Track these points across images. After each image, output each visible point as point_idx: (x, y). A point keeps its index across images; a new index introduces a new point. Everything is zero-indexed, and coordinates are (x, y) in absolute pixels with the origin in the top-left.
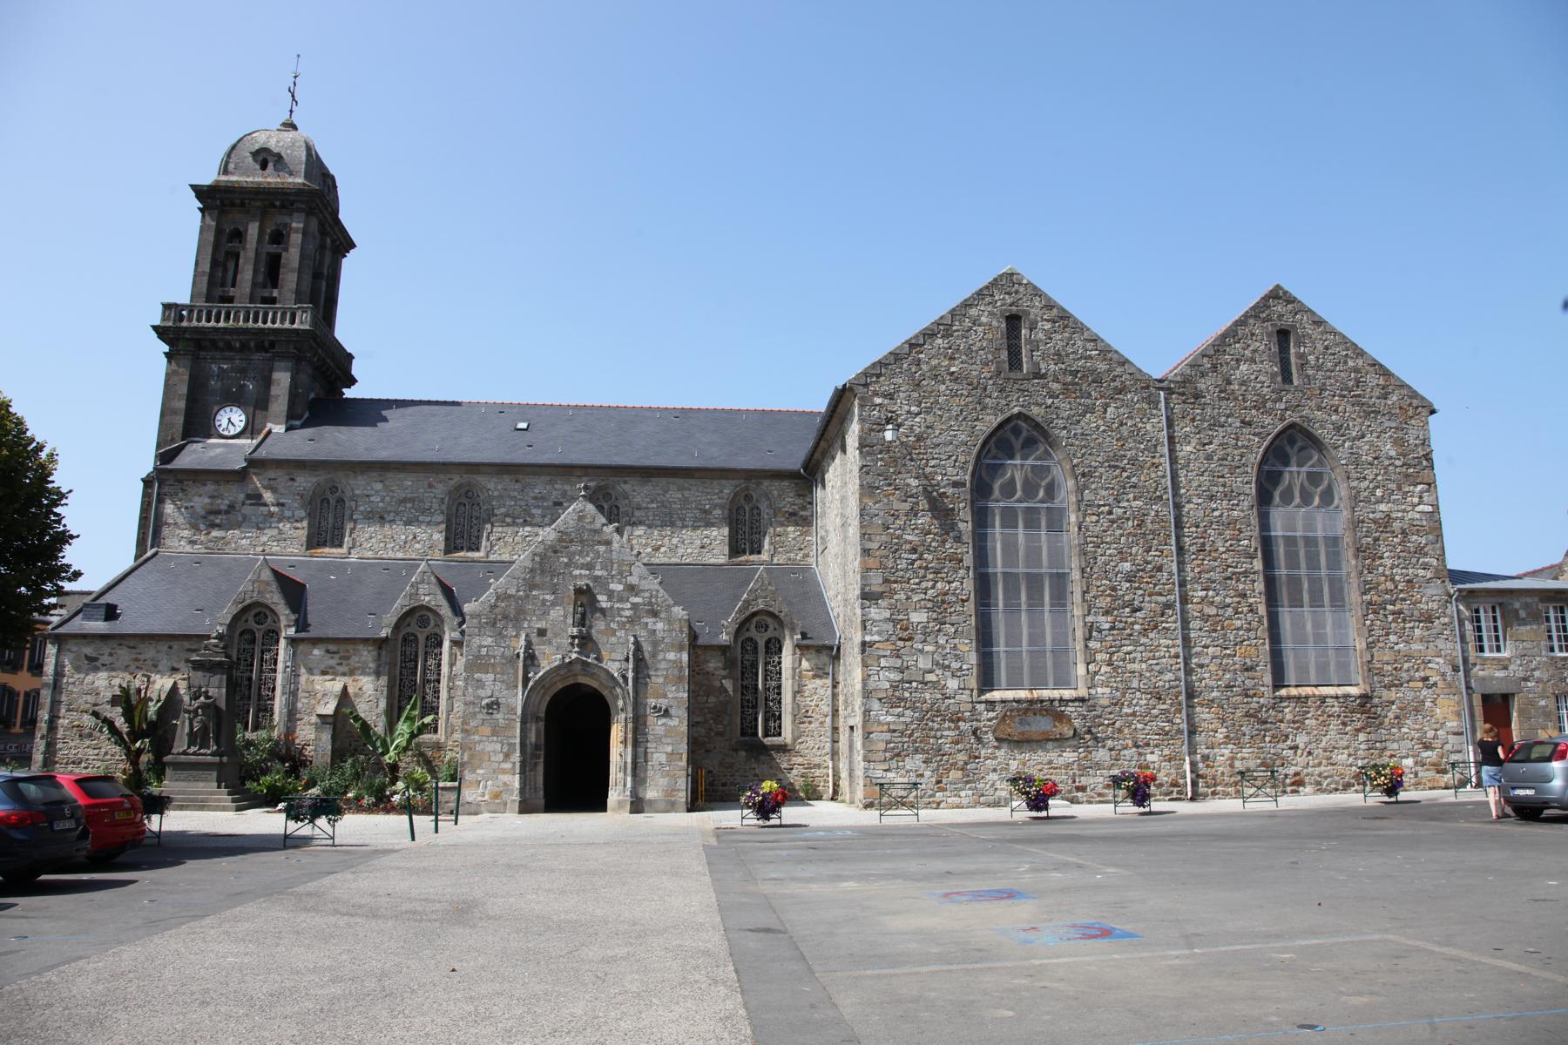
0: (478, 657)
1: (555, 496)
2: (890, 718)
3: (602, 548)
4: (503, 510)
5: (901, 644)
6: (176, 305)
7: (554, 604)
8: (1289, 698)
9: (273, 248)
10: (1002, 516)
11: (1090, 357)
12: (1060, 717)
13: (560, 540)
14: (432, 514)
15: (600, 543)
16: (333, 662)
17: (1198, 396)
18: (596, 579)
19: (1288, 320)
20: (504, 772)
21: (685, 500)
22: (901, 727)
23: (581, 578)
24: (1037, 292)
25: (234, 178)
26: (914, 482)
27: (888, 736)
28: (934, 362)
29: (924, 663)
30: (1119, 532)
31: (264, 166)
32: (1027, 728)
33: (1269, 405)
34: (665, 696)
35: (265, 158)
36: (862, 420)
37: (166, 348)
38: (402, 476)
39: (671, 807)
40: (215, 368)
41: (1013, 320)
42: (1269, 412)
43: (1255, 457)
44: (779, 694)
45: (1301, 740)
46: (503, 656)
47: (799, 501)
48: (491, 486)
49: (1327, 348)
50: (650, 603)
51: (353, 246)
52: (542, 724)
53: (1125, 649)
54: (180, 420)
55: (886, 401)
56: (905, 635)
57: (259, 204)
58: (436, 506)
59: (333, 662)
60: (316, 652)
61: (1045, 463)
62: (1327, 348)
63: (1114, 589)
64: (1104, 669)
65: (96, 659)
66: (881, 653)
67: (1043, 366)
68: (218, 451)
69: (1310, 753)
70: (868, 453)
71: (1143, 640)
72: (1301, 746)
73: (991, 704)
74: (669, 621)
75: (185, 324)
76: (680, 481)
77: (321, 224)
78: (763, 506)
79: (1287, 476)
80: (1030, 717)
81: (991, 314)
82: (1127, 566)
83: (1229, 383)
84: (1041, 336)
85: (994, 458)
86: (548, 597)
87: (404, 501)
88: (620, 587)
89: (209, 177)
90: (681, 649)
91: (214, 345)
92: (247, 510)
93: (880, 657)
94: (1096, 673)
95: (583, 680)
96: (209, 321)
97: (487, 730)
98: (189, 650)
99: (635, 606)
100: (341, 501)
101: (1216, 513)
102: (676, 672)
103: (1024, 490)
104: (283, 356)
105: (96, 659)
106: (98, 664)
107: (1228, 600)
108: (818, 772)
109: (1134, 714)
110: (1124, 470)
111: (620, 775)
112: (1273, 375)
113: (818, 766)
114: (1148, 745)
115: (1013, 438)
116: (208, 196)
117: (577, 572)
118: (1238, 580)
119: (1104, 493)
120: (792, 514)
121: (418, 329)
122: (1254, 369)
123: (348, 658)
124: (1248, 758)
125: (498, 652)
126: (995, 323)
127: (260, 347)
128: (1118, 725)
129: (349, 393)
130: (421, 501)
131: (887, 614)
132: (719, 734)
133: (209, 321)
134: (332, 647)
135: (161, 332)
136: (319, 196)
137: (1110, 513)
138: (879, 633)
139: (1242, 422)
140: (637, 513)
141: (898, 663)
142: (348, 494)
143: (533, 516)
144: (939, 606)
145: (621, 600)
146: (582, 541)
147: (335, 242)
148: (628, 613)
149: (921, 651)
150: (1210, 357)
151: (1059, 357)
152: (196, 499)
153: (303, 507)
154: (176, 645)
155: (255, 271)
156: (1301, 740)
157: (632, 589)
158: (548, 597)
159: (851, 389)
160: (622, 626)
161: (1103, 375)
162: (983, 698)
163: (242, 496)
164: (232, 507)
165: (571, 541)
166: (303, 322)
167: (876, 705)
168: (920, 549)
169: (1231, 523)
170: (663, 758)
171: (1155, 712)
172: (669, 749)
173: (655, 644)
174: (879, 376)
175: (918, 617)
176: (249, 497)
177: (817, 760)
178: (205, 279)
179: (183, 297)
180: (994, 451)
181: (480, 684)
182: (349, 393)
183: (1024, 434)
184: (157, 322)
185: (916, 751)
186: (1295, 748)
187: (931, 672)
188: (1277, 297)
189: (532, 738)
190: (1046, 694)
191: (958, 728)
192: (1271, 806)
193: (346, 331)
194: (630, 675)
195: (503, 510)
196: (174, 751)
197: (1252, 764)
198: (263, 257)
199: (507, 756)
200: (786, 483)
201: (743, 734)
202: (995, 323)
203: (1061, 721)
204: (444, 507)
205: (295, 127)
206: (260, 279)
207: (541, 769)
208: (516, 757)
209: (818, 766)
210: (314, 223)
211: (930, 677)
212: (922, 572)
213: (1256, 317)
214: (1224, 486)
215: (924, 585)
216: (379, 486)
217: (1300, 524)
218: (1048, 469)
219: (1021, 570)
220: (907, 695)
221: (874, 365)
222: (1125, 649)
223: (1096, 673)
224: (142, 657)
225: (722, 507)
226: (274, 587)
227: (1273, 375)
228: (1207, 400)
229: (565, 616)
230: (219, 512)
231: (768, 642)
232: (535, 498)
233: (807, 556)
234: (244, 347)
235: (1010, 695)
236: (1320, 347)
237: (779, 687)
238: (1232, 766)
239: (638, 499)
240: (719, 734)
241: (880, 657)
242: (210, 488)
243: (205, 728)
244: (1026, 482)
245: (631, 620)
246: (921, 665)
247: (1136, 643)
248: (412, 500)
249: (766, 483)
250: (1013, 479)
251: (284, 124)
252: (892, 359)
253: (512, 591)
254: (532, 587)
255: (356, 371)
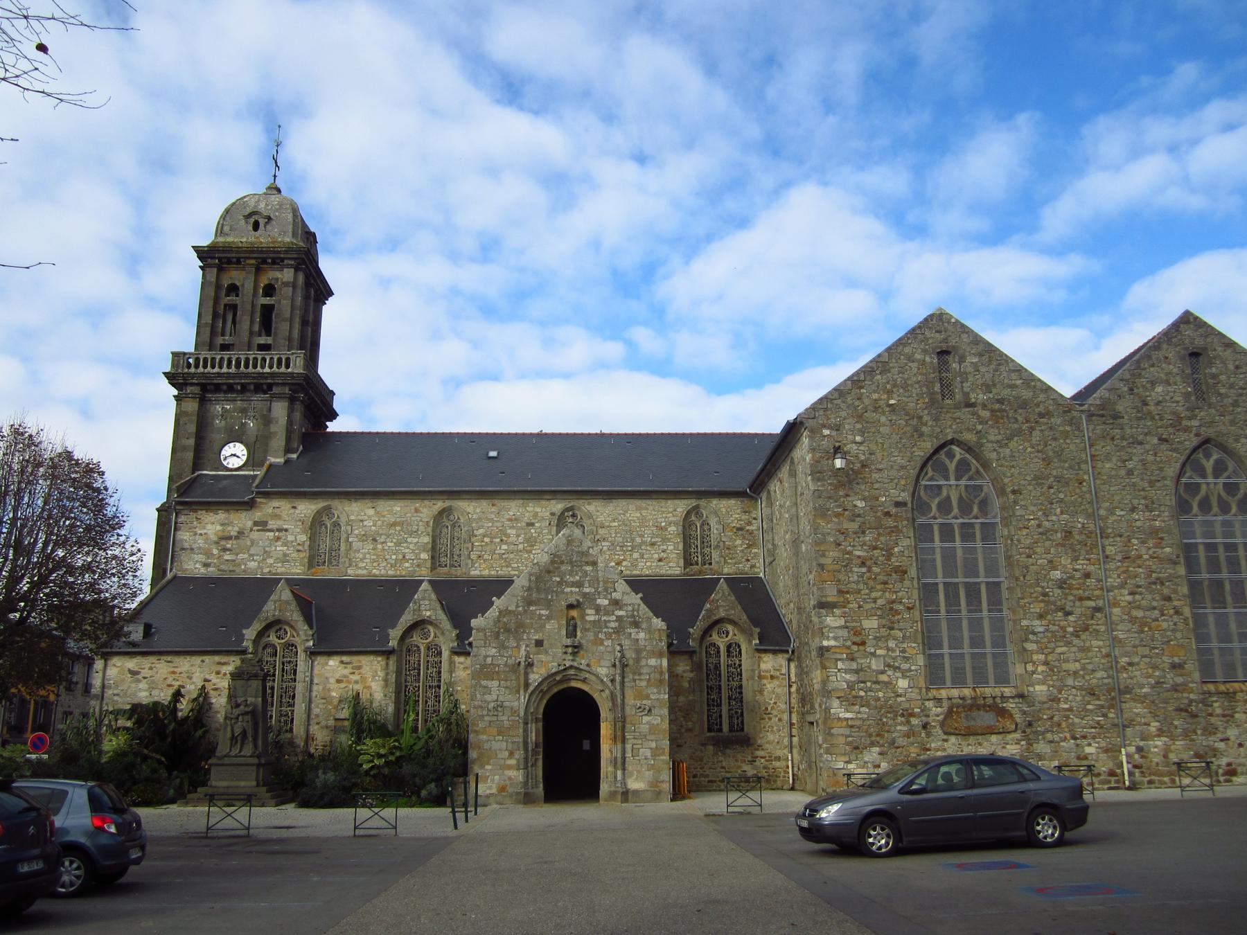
0: (484, 666)
1: (527, 517)
2: (848, 715)
3: (589, 568)
4: (481, 531)
5: (855, 648)
6: (185, 354)
7: (549, 618)
8: (1218, 693)
9: (266, 301)
10: (941, 532)
11: (1015, 386)
12: (1003, 713)
13: (553, 562)
14: (419, 536)
15: (587, 563)
16: (346, 672)
17: (1117, 416)
18: (585, 595)
19: (1199, 342)
20: (510, 767)
21: (643, 520)
22: (858, 723)
23: (572, 594)
24: (964, 329)
25: (230, 239)
26: (860, 504)
27: (847, 731)
28: (875, 396)
29: (875, 665)
30: (1047, 543)
31: (256, 226)
32: (973, 723)
33: (1185, 423)
34: (648, 697)
35: (256, 221)
36: (812, 450)
37: (176, 392)
38: (392, 502)
39: (657, 795)
40: (219, 408)
41: (941, 354)
42: (1187, 430)
43: (1172, 471)
44: (741, 693)
45: (1232, 733)
46: (506, 665)
47: (745, 517)
48: (470, 509)
49: (1237, 367)
50: (633, 616)
51: (331, 293)
52: (540, 724)
53: (1059, 650)
54: (190, 455)
55: (834, 433)
56: (857, 639)
57: (253, 261)
58: (422, 528)
59: (346, 672)
60: (331, 663)
61: (978, 483)
62: (1237, 367)
63: (1045, 595)
64: (1040, 668)
65: (137, 673)
66: (838, 656)
67: (972, 396)
68: (225, 482)
69: (1240, 745)
70: (819, 480)
71: (1076, 641)
72: (1232, 738)
73: (938, 701)
74: (649, 630)
75: (193, 370)
76: (639, 502)
77: (307, 277)
78: (713, 522)
79: (1204, 487)
80: (975, 714)
81: (925, 351)
82: (1057, 574)
83: (1146, 404)
84: (970, 369)
85: (931, 479)
86: (543, 612)
87: (394, 524)
88: (606, 602)
89: (205, 242)
90: (661, 655)
91: (217, 388)
92: (255, 535)
93: (837, 660)
94: (1034, 672)
95: (574, 684)
96: (213, 367)
97: (494, 731)
98: (219, 663)
99: (619, 619)
100: (337, 525)
101: (1138, 524)
102: (657, 676)
103: (959, 507)
104: (280, 397)
105: (137, 673)
106: (140, 677)
107: (1155, 604)
108: (777, 764)
109: (1070, 710)
110: (1051, 487)
111: (610, 769)
112: (1187, 396)
113: (778, 759)
114: (1084, 737)
115: (947, 461)
116: (203, 254)
117: (568, 590)
118: (1162, 584)
119: (1033, 508)
120: (739, 529)
121: (383, 363)
122: (1168, 392)
123: (359, 668)
124: (1180, 750)
125: (501, 661)
126: (928, 359)
127: (258, 389)
128: (1056, 719)
129: (332, 427)
130: (410, 524)
131: (841, 622)
132: (690, 730)
133: (213, 367)
134: (345, 658)
135: (171, 377)
136: (304, 256)
137: (1039, 526)
138: (835, 639)
139: (1160, 439)
140: (601, 531)
141: (854, 666)
142: (343, 520)
143: (508, 536)
144: (889, 612)
145: (607, 613)
146: (571, 563)
147: (318, 291)
148: (613, 625)
149: (873, 654)
150: (1127, 381)
151: (987, 388)
152: (209, 527)
153: (304, 532)
154: (207, 659)
155: (252, 322)
156: (1232, 733)
157: (616, 603)
158: (543, 612)
159: (802, 423)
160: (608, 636)
161: (1022, 396)
162: (930, 695)
163: (250, 523)
164: (241, 532)
165: (562, 562)
166: (297, 366)
167: (836, 703)
168: (868, 563)
169: (1154, 532)
170: (648, 753)
171: (1090, 707)
172: (653, 745)
173: (638, 651)
174: (826, 409)
175: (871, 624)
176: (256, 524)
177: (778, 753)
178: (208, 330)
179: (190, 347)
180: (930, 473)
181: (487, 690)
182: (332, 427)
183: (958, 457)
184: (168, 369)
185: (873, 744)
186: (1226, 740)
187: (883, 672)
188: (1188, 322)
189: (533, 737)
190: (988, 691)
191: (908, 722)
192: (1174, 793)
193: (328, 370)
194: (618, 678)
195: (481, 531)
196: (218, 754)
197: (1185, 756)
198: (258, 309)
199: (511, 754)
200: (732, 502)
201: (710, 730)
202: (928, 359)
203: (1003, 716)
204: (430, 529)
205: (279, 191)
206: (256, 328)
207: (540, 763)
208: (519, 754)
209: (778, 759)
210: (301, 277)
211: (884, 678)
212: (871, 583)
213: (1169, 341)
214: (1145, 498)
215: (874, 595)
216: (371, 512)
217: (1218, 529)
218: (980, 488)
219: (960, 579)
220: (862, 693)
221: (821, 399)
222: (1059, 650)
223: (1034, 672)
224: (178, 670)
225: (676, 524)
226: (294, 604)
227: (1187, 396)
228: (1125, 420)
229: (559, 629)
230: (230, 538)
231: (729, 647)
232: (510, 520)
233: (753, 566)
234: (244, 389)
235: (955, 693)
236: (1231, 367)
237: (741, 687)
238: (1165, 756)
239: (601, 519)
240: (690, 730)
241: (837, 660)
242: (221, 516)
243: (244, 733)
244: (961, 499)
245: (617, 631)
246: (874, 667)
247: (1068, 644)
248: (401, 524)
249: (715, 501)
250: (948, 497)
251: (269, 188)
252: (836, 395)
253: (512, 608)
254: (529, 603)
255: (337, 405)
